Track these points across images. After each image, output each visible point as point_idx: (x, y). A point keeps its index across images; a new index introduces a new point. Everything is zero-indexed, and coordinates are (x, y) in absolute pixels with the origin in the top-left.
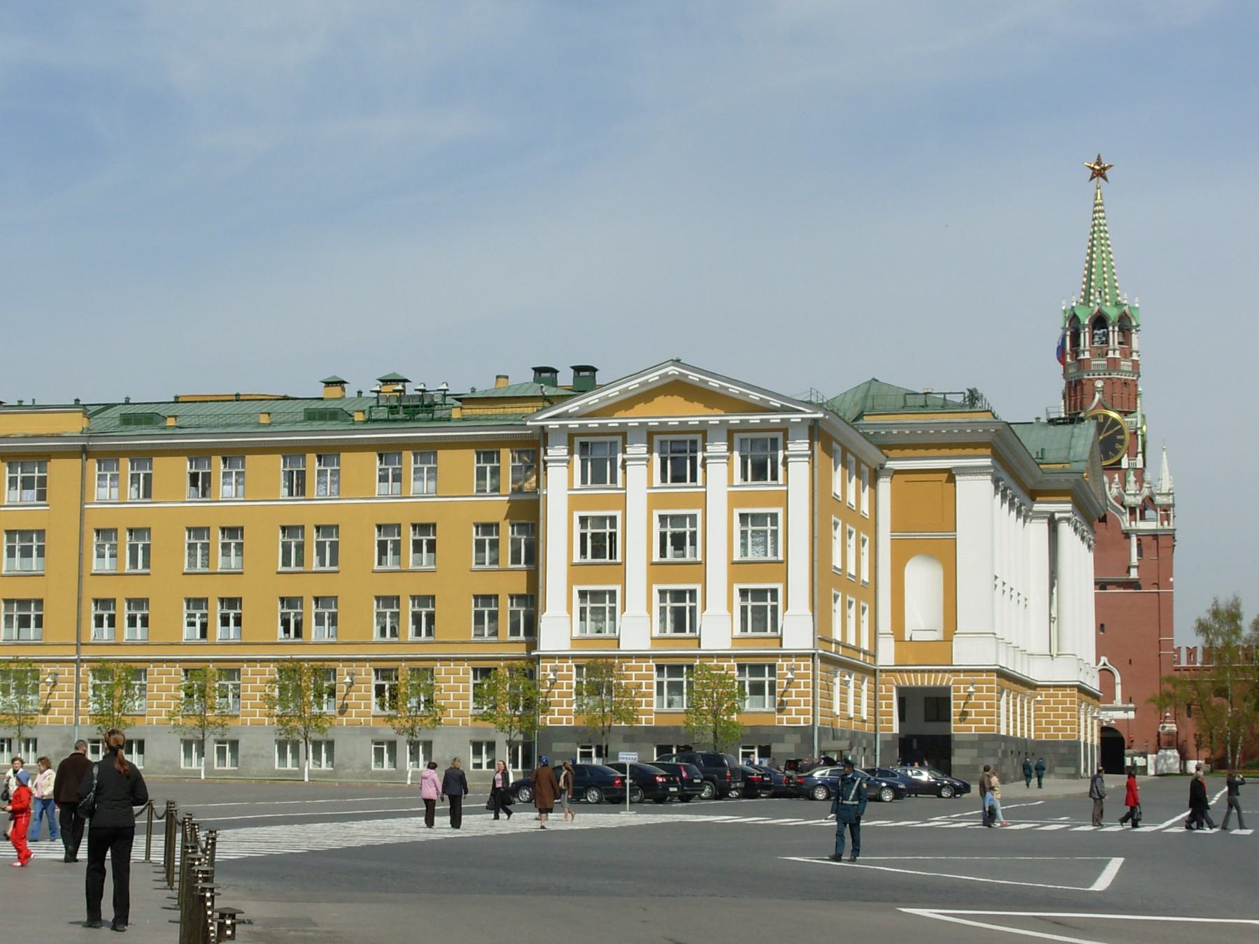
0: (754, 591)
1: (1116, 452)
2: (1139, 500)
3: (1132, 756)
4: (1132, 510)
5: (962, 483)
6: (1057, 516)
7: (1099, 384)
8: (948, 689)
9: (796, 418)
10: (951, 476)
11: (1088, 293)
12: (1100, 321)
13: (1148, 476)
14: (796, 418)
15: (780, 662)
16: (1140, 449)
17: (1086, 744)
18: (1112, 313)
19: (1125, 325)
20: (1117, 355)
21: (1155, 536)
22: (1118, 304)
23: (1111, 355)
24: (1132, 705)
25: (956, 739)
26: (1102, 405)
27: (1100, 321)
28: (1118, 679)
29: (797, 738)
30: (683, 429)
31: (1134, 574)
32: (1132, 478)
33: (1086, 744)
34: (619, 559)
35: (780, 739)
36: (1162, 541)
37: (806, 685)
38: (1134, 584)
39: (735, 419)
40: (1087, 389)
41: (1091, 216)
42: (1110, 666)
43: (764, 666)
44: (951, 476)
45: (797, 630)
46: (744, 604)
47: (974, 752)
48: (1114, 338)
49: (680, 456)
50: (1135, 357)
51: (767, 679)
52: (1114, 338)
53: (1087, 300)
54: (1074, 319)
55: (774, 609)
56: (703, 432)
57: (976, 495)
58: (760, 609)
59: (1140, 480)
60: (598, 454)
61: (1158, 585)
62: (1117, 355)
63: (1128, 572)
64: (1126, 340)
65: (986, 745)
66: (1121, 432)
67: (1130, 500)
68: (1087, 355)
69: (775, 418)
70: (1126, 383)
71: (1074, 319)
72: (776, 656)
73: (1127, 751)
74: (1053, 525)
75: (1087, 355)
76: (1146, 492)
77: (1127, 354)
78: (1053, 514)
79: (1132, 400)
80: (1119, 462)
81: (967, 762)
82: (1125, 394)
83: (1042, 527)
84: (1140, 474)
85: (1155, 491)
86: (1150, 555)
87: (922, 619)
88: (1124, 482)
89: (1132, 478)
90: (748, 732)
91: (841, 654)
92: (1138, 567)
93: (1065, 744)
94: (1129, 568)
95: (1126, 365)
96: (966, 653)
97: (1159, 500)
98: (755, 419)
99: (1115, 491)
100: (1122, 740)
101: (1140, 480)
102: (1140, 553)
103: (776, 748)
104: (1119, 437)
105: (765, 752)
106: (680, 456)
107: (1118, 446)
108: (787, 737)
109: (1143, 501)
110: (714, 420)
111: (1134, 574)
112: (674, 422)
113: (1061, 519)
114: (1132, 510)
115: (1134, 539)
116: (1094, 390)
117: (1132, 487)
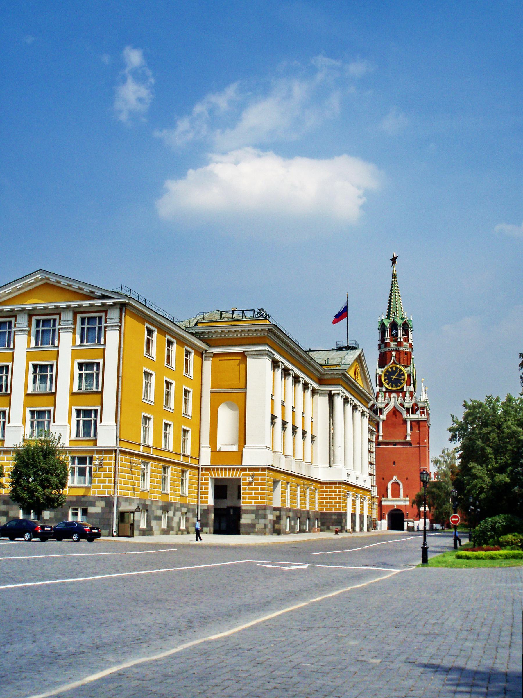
0: (85, 411)
1: (401, 384)
2: (411, 405)
3: (408, 522)
4: (408, 410)
5: (250, 361)
6: (333, 392)
7: (394, 353)
8: (239, 480)
9: (109, 302)
10: (244, 356)
11: (389, 313)
12: (394, 326)
13: (415, 395)
14: (109, 302)
15: (95, 456)
16: (412, 382)
17: (353, 515)
18: (400, 322)
19: (406, 328)
20: (402, 340)
21: (418, 422)
22: (403, 319)
23: (399, 340)
24: (408, 499)
25: (243, 508)
26: (394, 363)
27: (394, 326)
28: (401, 487)
29: (103, 504)
30: (45, 311)
31: (409, 439)
32: (408, 395)
33: (353, 515)
34: (9, 392)
35: (93, 504)
36: (421, 423)
37: (110, 471)
38: (409, 443)
39: (74, 304)
40: (388, 355)
41: (391, 280)
42: (398, 481)
43: (86, 458)
44: (244, 356)
45: (107, 435)
46: (79, 419)
47: (253, 516)
48: (400, 333)
49: (45, 327)
50: (410, 341)
51: (88, 466)
52: (400, 333)
53: (388, 316)
54: (383, 325)
55: (96, 421)
56: (57, 311)
57: (260, 370)
58: (88, 419)
59: (411, 396)
60: (91, 327)
61: (419, 444)
62: (402, 340)
63: (406, 438)
64: (406, 334)
65: (260, 512)
66: (403, 374)
67: (406, 405)
68: (388, 341)
69: (98, 303)
70: (406, 353)
71: (383, 325)
72: (92, 451)
73: (405, 520)
74: (331, 397)
75: (388, 341)
76: (413, 401)
77: (407, 340)
78: (331, 391)
79: (408, 361)
80: (403, 388)
81: (249, 522)
82: (406, 358)
83: (325, 399)
84: (412, 394)
85: (418, 400)
86: (416, 430)
87: (226, 439)
88: (404, 396)
89: (408, 395)
90: (74, 499)
91: (152, 453)
92: (410, 435)
93: (335, 514)
94: (406, 436)
95: (406, 344)
96: (250, 458)
97: (420, 405)
98: (86, 303)
99: (400, 401)
100: (403, 514)
101: (411, 396)
102: (411, 429)
103: (91, 510)
104: (390, 370)
105: (85, 512)
106: (45, 327)
107: (402, 381)
108: (97, 503)
109: (413, 405)
110: (63, 305)
111: (409, 439)
112: (40, 307)
113: (334, 394)
114: (408, 410)
115: (409, 423)
116: (391, 356)
117: (408, 398)
